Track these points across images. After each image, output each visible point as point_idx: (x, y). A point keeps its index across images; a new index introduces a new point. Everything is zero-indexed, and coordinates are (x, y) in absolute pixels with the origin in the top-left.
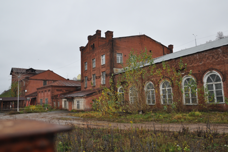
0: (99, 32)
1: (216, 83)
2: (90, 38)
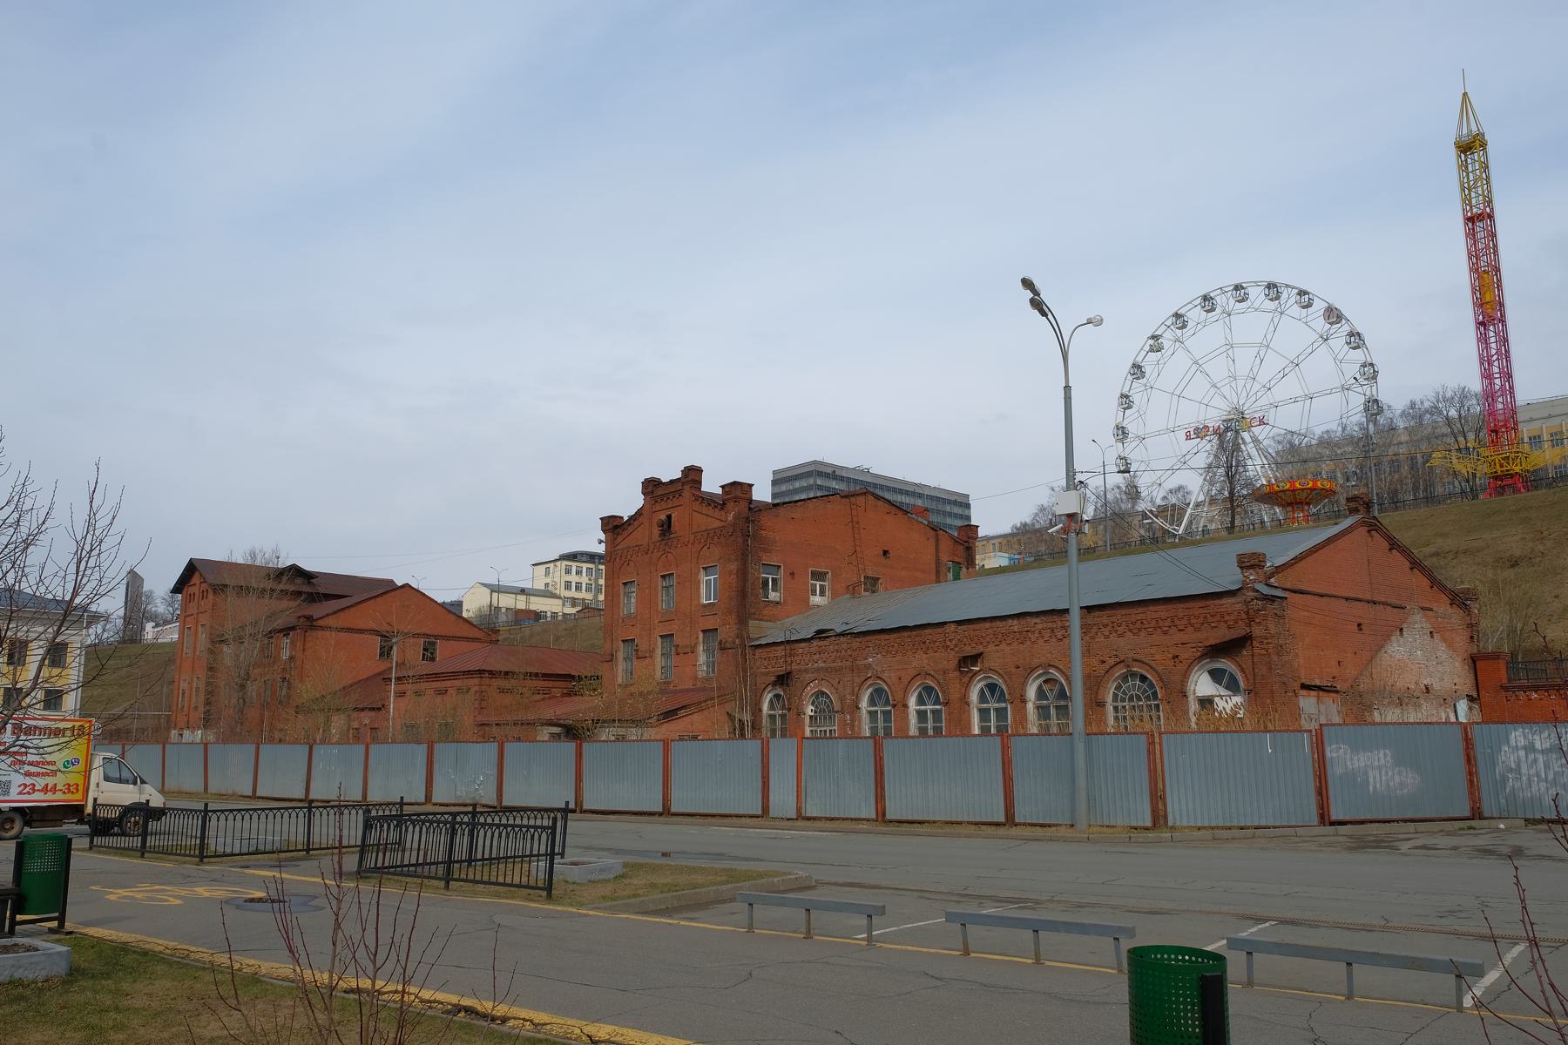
0: (692, 475)
1: (997, 705)
2: (652, 487)
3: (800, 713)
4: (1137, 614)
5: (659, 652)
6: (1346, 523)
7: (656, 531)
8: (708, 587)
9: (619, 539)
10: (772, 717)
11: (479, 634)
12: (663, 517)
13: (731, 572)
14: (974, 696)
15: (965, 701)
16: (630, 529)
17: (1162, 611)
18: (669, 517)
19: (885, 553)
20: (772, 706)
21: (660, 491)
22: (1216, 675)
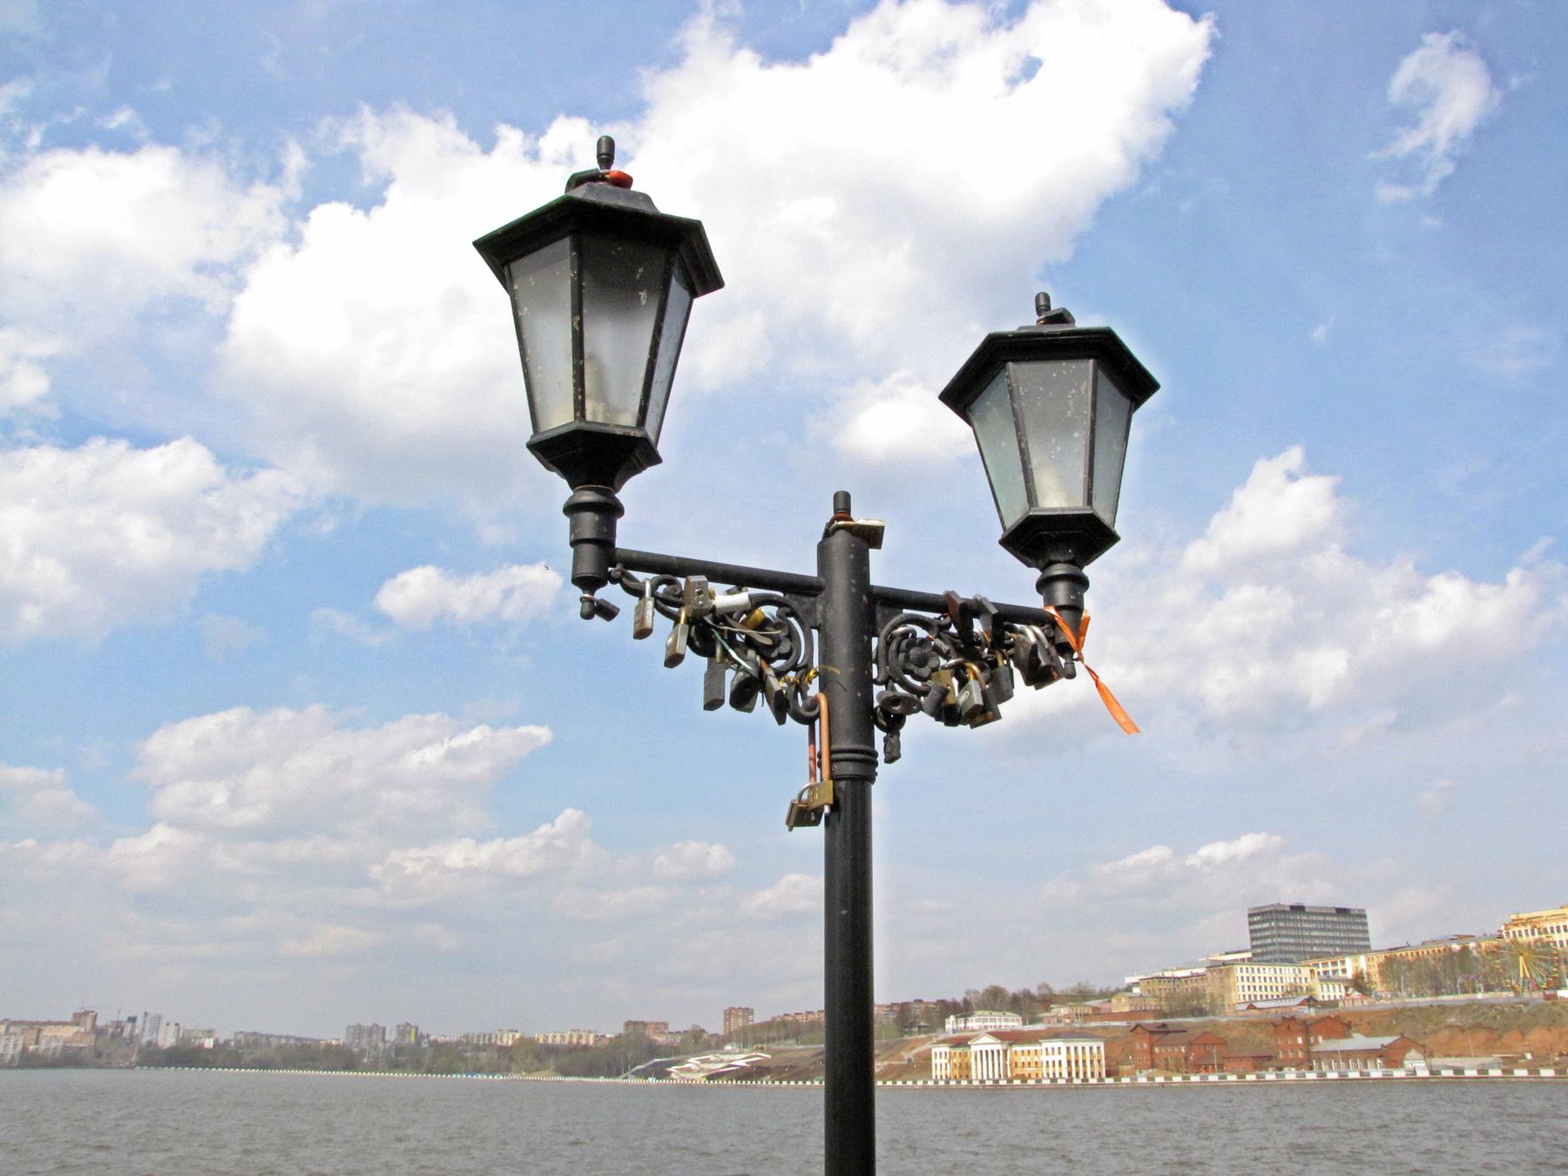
8: (1300, 1041)
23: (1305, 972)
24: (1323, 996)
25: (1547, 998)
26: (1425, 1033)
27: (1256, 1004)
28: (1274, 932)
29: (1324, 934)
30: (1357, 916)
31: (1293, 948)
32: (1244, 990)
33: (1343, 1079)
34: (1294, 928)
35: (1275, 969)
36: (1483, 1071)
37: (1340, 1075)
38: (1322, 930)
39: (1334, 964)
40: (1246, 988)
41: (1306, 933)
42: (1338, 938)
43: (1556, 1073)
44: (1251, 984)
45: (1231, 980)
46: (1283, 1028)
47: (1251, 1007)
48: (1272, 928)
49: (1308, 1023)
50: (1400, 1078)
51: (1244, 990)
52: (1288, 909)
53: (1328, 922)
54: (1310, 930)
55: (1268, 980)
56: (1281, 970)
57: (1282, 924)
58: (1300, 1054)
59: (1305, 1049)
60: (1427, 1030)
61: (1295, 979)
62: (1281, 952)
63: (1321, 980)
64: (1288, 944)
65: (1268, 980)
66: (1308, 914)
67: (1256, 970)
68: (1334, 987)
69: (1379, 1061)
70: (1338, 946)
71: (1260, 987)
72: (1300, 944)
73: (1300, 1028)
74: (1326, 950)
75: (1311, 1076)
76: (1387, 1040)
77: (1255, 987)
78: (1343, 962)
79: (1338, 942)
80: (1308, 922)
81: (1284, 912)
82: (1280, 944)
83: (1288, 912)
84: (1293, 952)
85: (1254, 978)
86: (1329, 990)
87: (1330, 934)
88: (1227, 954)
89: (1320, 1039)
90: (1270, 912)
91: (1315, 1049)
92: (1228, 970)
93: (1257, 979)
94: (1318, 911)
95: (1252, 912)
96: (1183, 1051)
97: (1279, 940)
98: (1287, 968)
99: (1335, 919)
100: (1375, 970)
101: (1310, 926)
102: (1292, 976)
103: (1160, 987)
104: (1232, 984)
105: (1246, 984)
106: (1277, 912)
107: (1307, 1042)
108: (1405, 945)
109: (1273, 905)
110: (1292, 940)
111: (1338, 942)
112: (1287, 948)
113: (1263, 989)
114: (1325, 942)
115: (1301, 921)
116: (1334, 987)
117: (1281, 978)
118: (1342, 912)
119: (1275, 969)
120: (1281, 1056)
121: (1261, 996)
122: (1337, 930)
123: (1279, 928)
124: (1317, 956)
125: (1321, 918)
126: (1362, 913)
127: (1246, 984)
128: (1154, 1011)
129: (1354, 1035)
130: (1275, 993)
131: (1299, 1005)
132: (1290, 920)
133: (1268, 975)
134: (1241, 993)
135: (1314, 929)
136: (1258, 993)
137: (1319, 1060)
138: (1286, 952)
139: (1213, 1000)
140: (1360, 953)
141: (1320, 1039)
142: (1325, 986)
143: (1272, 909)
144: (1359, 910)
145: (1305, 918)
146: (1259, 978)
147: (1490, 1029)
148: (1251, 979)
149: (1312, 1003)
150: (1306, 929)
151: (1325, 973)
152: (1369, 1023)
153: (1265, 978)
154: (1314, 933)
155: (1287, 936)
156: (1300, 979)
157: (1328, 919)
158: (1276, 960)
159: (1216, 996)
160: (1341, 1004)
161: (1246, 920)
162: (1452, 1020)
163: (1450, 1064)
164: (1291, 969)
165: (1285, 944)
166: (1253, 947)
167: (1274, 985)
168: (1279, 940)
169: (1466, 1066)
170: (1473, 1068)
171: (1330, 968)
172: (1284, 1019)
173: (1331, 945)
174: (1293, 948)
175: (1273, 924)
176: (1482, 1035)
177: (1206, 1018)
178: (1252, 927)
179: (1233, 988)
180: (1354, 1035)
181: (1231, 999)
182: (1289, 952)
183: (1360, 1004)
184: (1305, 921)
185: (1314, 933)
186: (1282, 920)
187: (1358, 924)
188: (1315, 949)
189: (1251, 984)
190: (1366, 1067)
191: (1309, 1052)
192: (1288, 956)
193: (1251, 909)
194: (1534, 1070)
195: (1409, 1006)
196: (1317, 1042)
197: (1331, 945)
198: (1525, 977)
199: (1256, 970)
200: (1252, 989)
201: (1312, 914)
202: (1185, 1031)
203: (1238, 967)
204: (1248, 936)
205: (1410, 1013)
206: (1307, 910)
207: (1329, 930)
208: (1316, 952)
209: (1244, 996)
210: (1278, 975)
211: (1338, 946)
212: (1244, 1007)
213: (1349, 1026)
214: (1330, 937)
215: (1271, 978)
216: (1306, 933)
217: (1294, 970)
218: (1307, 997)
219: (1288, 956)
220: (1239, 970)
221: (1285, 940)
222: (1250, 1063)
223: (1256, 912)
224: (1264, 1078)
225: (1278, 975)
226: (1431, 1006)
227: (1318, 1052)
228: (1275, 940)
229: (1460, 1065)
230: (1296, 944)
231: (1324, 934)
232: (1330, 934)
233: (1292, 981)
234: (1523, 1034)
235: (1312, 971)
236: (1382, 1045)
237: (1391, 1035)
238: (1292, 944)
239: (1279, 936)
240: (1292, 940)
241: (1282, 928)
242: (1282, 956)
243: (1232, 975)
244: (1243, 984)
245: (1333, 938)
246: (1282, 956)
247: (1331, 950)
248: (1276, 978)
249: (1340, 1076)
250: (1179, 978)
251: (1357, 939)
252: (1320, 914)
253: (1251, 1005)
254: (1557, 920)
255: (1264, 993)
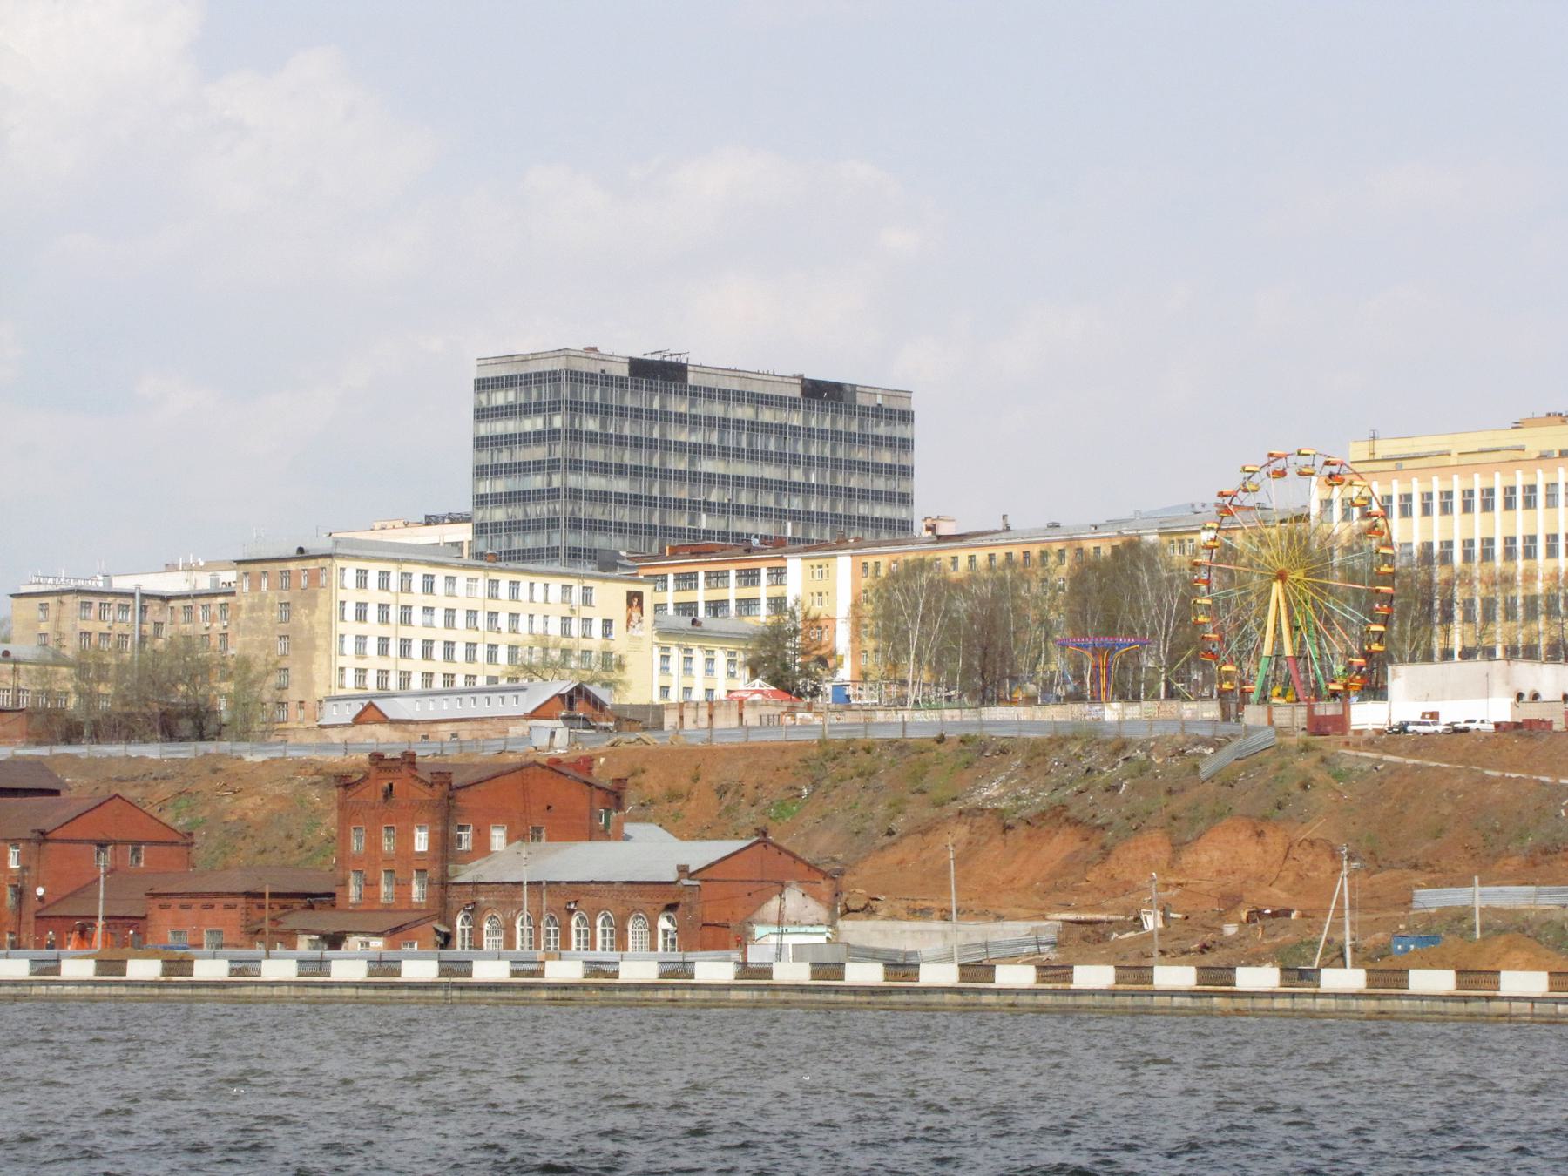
3: (482, 929)
4: (642, 888)
5: (383, 881)
6: (755, 839)
7: (381, 795)
8: (421, 841)
9: (350, 793)
10: (463, 931)
11: (176, 838)
12: (386, 784)
13: (436, 833)
14: (573, 923)
15: (569, 927)
16: (359, 787)
17: (650, 888)
18: (391, 785)
19: (549, 807)
20: (463, 924)
21: (383, 764)
22: (669, 918)
23: (610, 596)
24: (665, 690)
25: (1318, 726)
26: (890, 833)
27: (390, 708)
28: (560, 451)
29: (744, 469)
30: (879, 413)
31: (624, 515)
32: (361, 653)
33: (526, 982)
34: (636, 443)
35: (494, 583)
36: (977, 971)
37: (594, 968)
38: (738, 454)
39: (749, 577)
40: (372, 646)
41: (677, 463)
42: (795, 488)
43: (1041, 978)
44: (394, 632)
45: (320, 615)
46: (371, 794)
47: (369, 714)
48: (554, 435)
49: (457, 780)
50: (640, 987)
51: (361, 653)
52: (624, 371)
53: (767, 428)
54: (695, 450)
55: (460, 619)
56: (514, 585)
57: (592, 425)
58: (417, 892)
59: (434, 872)
60: (899, 823)
61: (566, 620)
62: (574, 524)
63: (665, 633)
64: (605, 497)
65: (460, 619)
66: (696, 392)
67: (417, 583)
68: (710, 661)
69: (663, 923)
70: (794, 516)
71: (471, 647)
72: (650, 502)
73: (423, 794)
74: (743, 526)
75: (714, 970)
76: (702, 853)
77: (405, 645)
78: (778, 574)
79: (797, 503)
80: (695, 422)
81: (607, 380)
82: (574, 494)
83: (621, 381)
84: (621, 528)
85: (406, 611)
86: (687, 671)
87: (771, 472)
88: (430, 521)
89: (498, 838)
90: (554, 377)
91: (467, 874)
92: (314, 577)
93: (417, 616)
94: (735, 385)
95: (490, 373)
96: (13, 864)
97: (575, 481)
98: (539, 582)
99: (796, 419)
100: (841, 605)
101: (697, 438)
102: (557, 610)
103: (87, 627)
104: (319, 630)
105: (373, 628)
106: (575, 377)
107: (445, 847)
108: (1000, 527)
109: (565, 353)
110: (621, 485)
111: (797, 503)
112: (598, 512)
113: (438, 651)
114: (744, 498)
115: (666, 416)
116: (710, 661)
117: (514, 617)
118: (819, 392)
119: (494, 583)
120: (353, 892)
121: (428, 677)
122: (795, 460)
123: (575, 436)
124: (699, 546)
125: (745, 413)
126: (896, 404)
127: (373, 628)
128: (30, 714)
129: (628, 828)
130: (482, 671)
131: (534, 715)
132: (622, 412)
133: (461, 606)
134: (350, 662)
135: (709, 451)
136: (416, 665)
137: (474, 912)
138: (592, 525)
139: (246, 684)
140: (841, 543)
141: (498, 838)
142: (676, 655)
143: (558, 365)
144: (888, 393)
145: (679, 406)
146: (428, 610)
147: (1088, 828)
148: (394, 614)
149: (581, 709)
150: (681, 447)
151: (687, 608)
152: (722, 791)
153: (450, 613)
154: (707, 466)
155: (605, 469)
156: (587, 621)
157: (767, 416)
158: (552, 554)
159: (259, 667)
160: (670, 719)
161: (467, 401)
162: (991, 792)
163: (877, 943)
164: (556, 585)
165: (591, 496)
166: (480, 500)
167: (482, 638)
168: (575, 481)
169: (926, 950)
170: (948, 958)
171: (732, 592)
172: (377, 758)
173: (766, 513)
174: (624, 515)
175: (558, 422)
176: (1060, 846)
177: (211, 747)
178: (486, 429)
179: (320, 642)
180: (628, 828)
181: (309, 682)
182: (605, 527)
183: (735, 723)
184: (681, 419)
185: (707, 466)
186: (592, 409)
187: (878, 441)
188: (704, 522)
189: (394, 632)
190: (620, 942)
191: (445, 884)
192: (600, 541)
193: (484, 362)
194: (1387, 975)
195: (912, 734)
196: (482, 847)
197: (766, 513)
198: (1278, 654)
199: (417, 583)
200: (394, 648)
201: (710, 393)
202: (56, 793)
203: (351, 568)
204: (467, 458)
205: (865, 761)
206: (692, 379)
207: (767, 457)
208: (709, 533)
209: (361, 673)
210: (504, 606)
211: (794, 516)
212: (349, 712)
213: (615, 796)
214: (767, 484)
215: (471, 614)
216: (677, 463)
217: (567, 589)
218: (564, 687)
219: (600, 541)
220: (351, 578)
221: (596, 483)
222: (235, 916)
223: (503, 371)
224: (615, 975)
225: (504, 606)
226: (941, 740)
227: (475, 884)
228: (556, 481)
229: (907, 945)
230: (635, 500)
231: (744, 469)
232: (771, 472)
233: (555, 629)
234: (1177, 847)
235: (634, 599)
236: (683, 870)
237: (723, 836)
238: (621, 499)
239: (574, 466)
240: (621, 485)
241: (591, 438)
242: (578, 540)
243: (322, 596)
244: (361, 629)
245: (781, 486)
246: (578, 540)
247: (765, 528)
248: (493, 615)
249: (443, 972)
250: (165, 599)
251: (865, 495)
252: (740, 397)
253: (371, 705)
254: (1487, 469)
255: (438, 666)
